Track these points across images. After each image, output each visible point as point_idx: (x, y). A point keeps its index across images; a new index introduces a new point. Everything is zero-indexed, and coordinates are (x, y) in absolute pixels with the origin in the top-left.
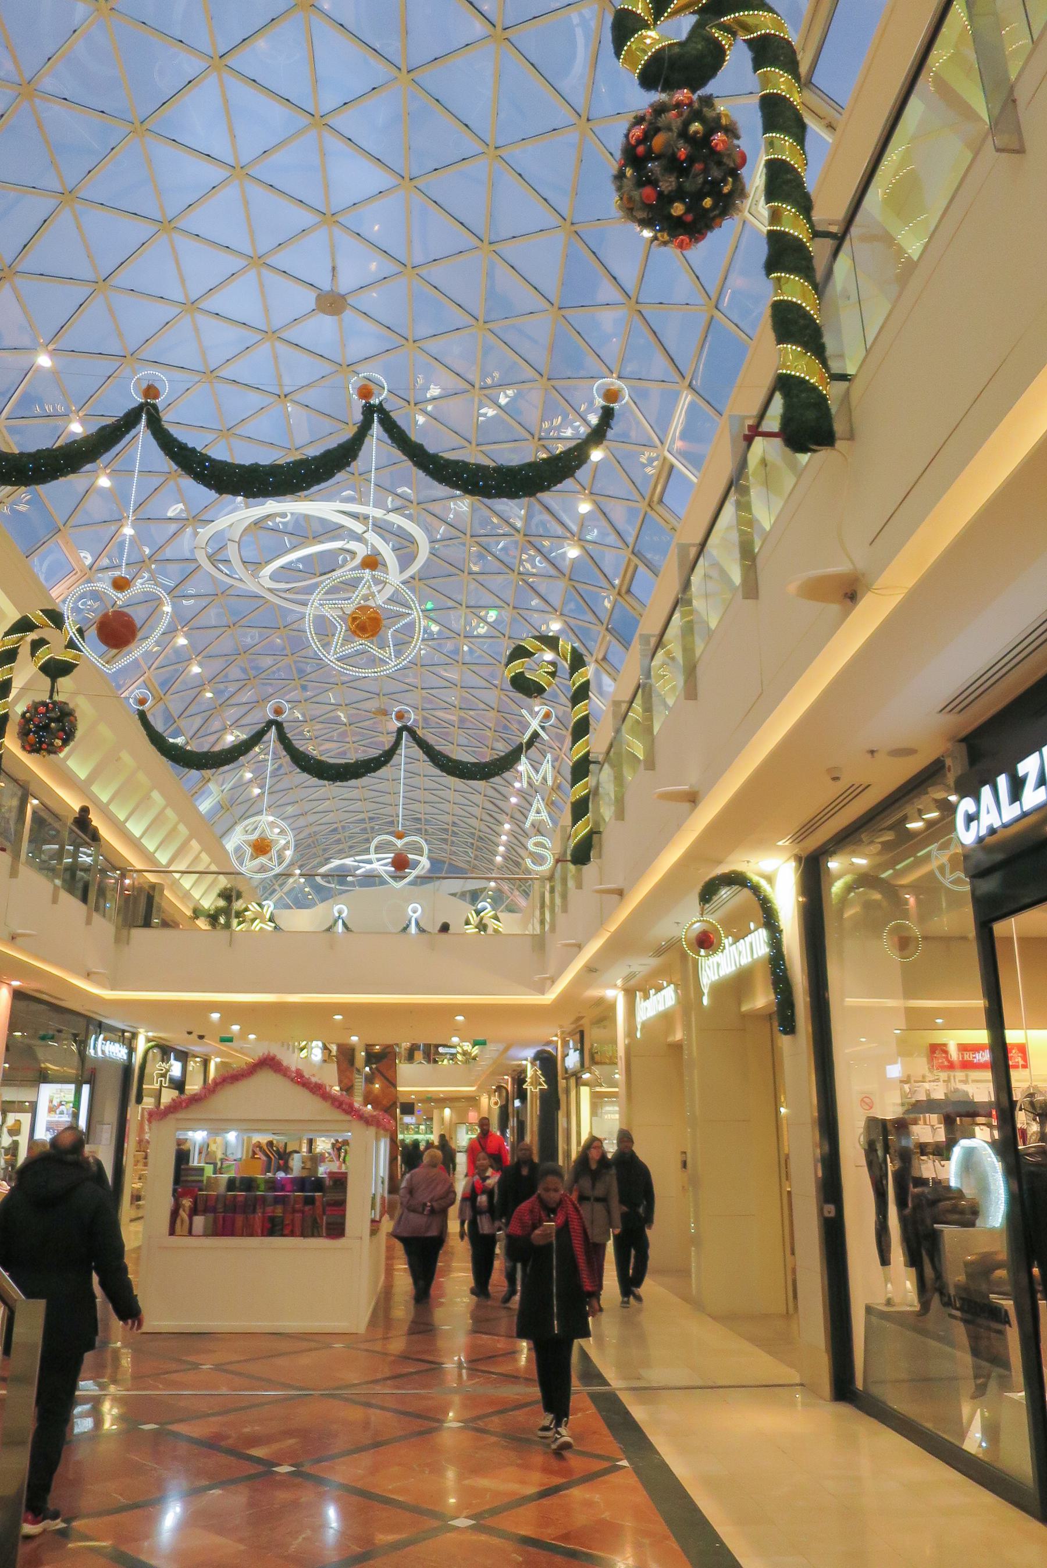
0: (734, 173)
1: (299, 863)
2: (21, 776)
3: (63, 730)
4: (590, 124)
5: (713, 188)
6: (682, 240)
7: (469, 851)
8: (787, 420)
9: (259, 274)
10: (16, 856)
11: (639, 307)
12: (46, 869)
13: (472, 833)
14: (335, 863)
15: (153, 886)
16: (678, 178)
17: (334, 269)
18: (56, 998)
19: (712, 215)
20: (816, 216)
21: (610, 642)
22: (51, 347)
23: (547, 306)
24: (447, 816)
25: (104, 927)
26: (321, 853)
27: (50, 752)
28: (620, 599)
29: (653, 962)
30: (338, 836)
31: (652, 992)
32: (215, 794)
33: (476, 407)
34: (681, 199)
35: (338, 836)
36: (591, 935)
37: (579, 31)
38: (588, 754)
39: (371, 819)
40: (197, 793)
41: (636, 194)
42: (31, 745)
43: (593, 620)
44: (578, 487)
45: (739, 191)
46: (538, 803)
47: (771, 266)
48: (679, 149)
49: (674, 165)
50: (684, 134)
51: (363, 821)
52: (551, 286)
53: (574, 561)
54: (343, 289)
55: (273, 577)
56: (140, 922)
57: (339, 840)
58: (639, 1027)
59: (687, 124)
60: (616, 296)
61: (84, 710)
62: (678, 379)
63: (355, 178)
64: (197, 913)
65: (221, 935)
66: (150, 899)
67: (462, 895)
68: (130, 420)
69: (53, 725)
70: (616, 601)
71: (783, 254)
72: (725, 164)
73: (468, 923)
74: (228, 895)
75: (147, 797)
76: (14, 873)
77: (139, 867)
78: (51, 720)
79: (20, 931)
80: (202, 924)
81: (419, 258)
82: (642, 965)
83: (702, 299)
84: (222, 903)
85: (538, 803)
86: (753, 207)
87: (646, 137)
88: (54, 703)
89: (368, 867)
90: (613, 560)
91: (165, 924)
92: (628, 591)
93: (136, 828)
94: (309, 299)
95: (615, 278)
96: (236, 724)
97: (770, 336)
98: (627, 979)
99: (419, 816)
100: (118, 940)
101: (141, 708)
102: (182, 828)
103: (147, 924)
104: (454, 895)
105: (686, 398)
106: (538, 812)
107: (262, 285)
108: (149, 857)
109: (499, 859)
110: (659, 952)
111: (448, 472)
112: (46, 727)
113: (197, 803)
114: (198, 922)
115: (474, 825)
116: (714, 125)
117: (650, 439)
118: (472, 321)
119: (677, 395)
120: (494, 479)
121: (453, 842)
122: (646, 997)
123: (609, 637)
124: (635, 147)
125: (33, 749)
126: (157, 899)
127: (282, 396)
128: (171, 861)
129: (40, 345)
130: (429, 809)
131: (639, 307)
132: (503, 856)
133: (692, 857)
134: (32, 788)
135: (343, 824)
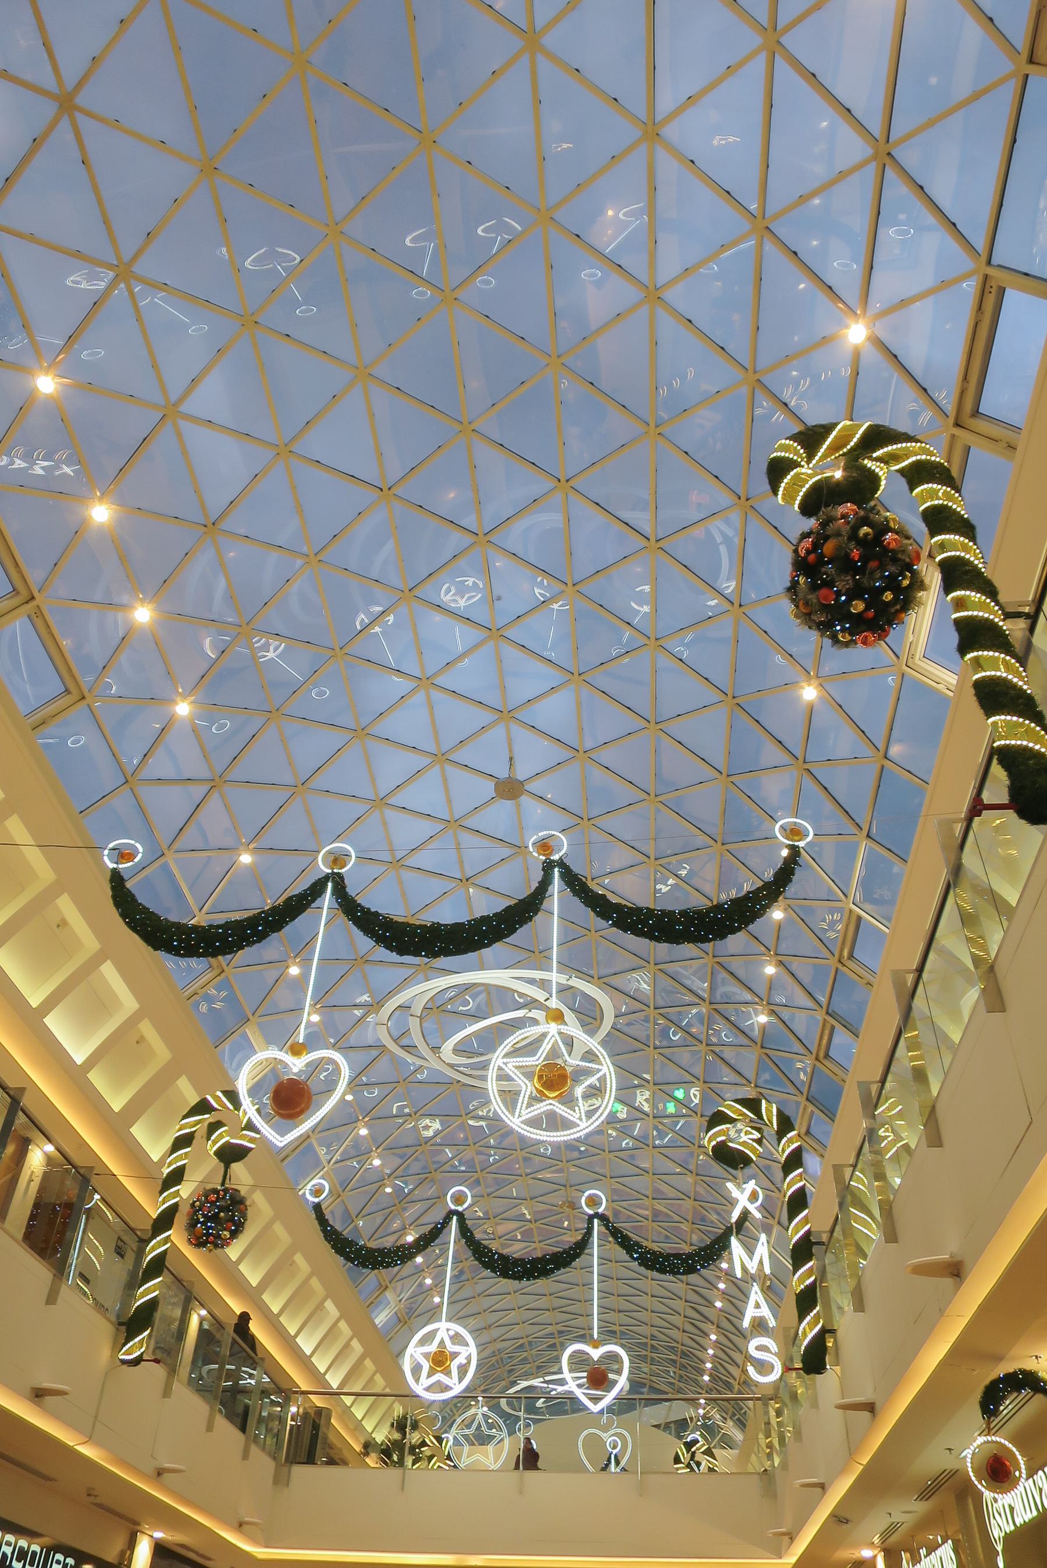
0: (909, 567)
1: (482, 1388)
2: (185, 1276)
3: (231, 1220)
4: (743, 609)
5: (892, 584)
6: (866, 637)
7: (671, 1370)
8: (1015, 791)
9: (443, 769)
10: (172, 1371)
11: (806, 766)
12: (201, 1388)
13: (673, 1347)
14: (524, 1384)
15: (319, 1411)
16: (854, 577)
17: (511, 759)
18: (197, 1553)
19: (893, 610)
20: (1001, 597)
21: (812, 1112)
22: (252, 846)
23: (716, 774)
24: (644, 1327)
25: (262, 1463)
26: (506, 1374)
27: (216, 1246)
28: (818, 1064)
29: (921, 1508)
30: (525, 1354)
31: (923, 1552)
32: (393, 1304)
33: (652, 882)
34: (860, 597)
35: (525, 1354)
36: (843, 1470)
37: (723, 549)
38: (808, 1233)
39: (560, 1332)
40: (372, 1304)
41: (812, 597)
42: (197, 1238)
43: (793, 1090)
44: (763, 948)
45: (917, 583)
46: (756, 1294)
47: (963, 649)
48: (852, 551)
49: (846, 565)
50: (853, 535)
51: (551, 1335)
52: (720, 759)
53: (764, 1028)
54: (521, 777)
55: (456, 1051)
56: (304, 1457)
57: (525, 1359)
58: (999, 1548)
59: (855, 529)
60: (782, 757)
61: (260, 1207)
62: (855, 831)
63: (529, 679)
64: (368, 1446)
65: (394, 1473)
66: (316, 1427)
67: (667, 1427)
68: (316, 890)
69: (222, 1214)
70: (814, 1067)
71: (973, 635)
72: (900, 560)
73: (677, 1460)
74: (400, 1426)
75: (320, 1307)
76: (167, 1392)
77: (304, 1388)
78: (221, 1209)
79: (167, 1465)
80: (372, 1461)
81: (589, 744)
82: (905, 1511)
83: (869, 751)
84: (397, 1436)
85: (756, 1294)
86: (910, 660)
87: (816, 546)
88: (226, 1191)
89: (560, 1389)
90: (806, 1022)
91: (332, 1462)
92: (827, 1056)
93: (306, 1344)
94: (488, 788)
95: (780, 742)
96: (415, 1222)
97: (980, 712)
98: (886, 1535)
99: (614, 1328)
100: (276, 1481)
101: (316, 1200)
102: (355, 1344)
103: (310, 1459)
104: (657, 1426)
105: (864, 845)
106: (757, 1306)
107: (445, 780)
108: (318, 1377)
109: (706, 1378)
110: (926, 1493)
111: (632, 920)
112: (215, 1218)
113: (373, 1316)
114: (367, 1460)
115: (674, 1337)
116: (884, 528)
117: (830, 891)
118: (644, 796)
119: (856, 846)
120: (681, 923)
121: (653, 1359)
122: (916, 1560)
123: (811, 1108)
124: (804, 559)
125: (199, 1242)
126: (323, 1429)
127: (464, 880)
128: (342, 1384)
129: (242, 844)
130: (623, 1319)
131: (806, 766)
132: (710, 1375)
133: (958, 1353)
134: (197, 1291)
135: (529, 1339)
